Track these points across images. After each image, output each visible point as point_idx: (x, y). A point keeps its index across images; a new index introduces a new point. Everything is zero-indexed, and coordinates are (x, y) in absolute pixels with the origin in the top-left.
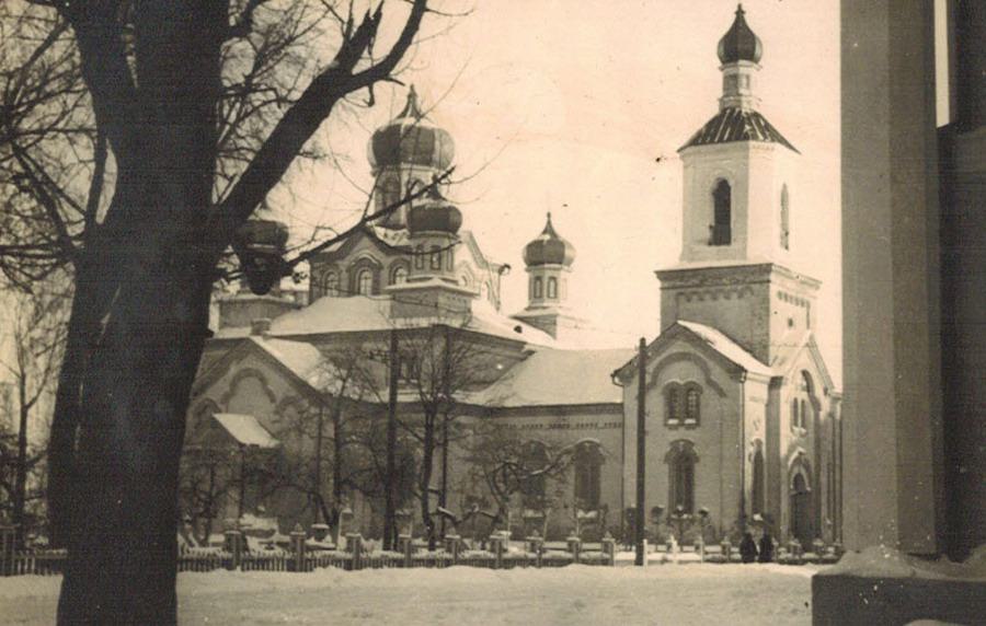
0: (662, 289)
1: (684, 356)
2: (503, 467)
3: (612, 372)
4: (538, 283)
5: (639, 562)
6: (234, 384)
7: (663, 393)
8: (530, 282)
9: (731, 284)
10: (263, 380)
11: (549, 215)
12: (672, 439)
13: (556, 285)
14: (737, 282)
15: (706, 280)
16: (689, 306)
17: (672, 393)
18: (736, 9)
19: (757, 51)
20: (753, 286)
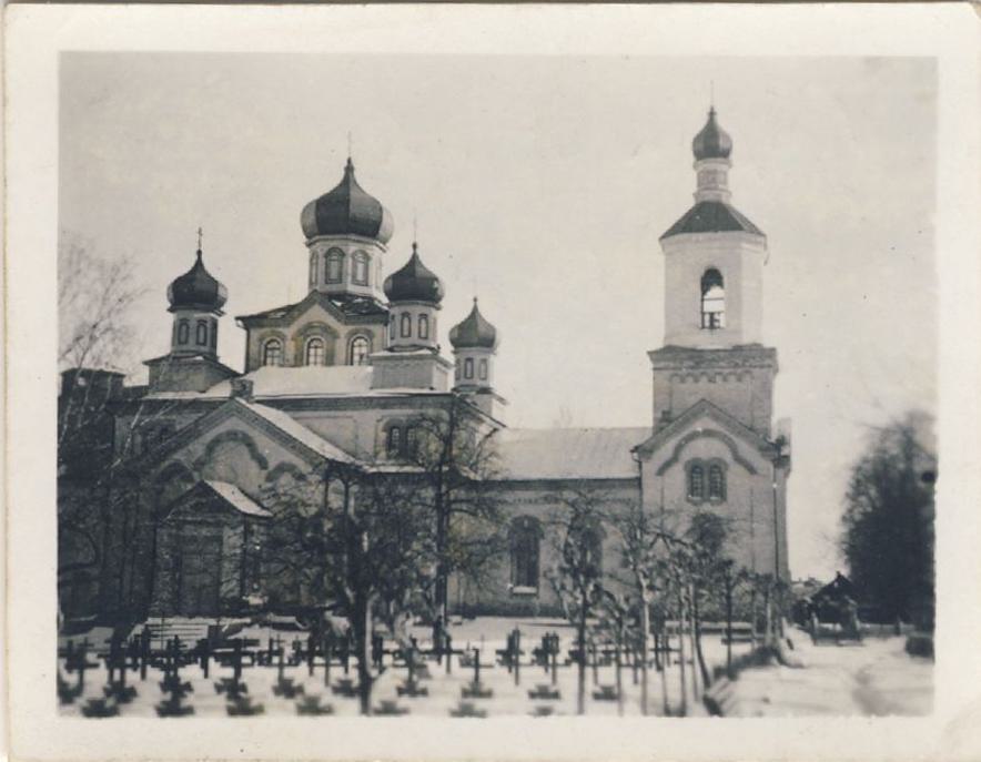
0: (655, 369)
1: (708, 433)
2: (658, 535)
3: (631, 448)
4: (423, 321)
5: (176, 636)
6: (210, 448)
7: (685, 467)
8: (435, 332)
9: (729, 367)
10: (250, 445)
11: (415, 246)
12: (724, 505)
13: (427, 323)
14: (737, 365)
15: (703, 362)
16: (683, 386)
17: (695, 469)
18: (709, 110)
19: (722, 143)
20: (752, 370)
